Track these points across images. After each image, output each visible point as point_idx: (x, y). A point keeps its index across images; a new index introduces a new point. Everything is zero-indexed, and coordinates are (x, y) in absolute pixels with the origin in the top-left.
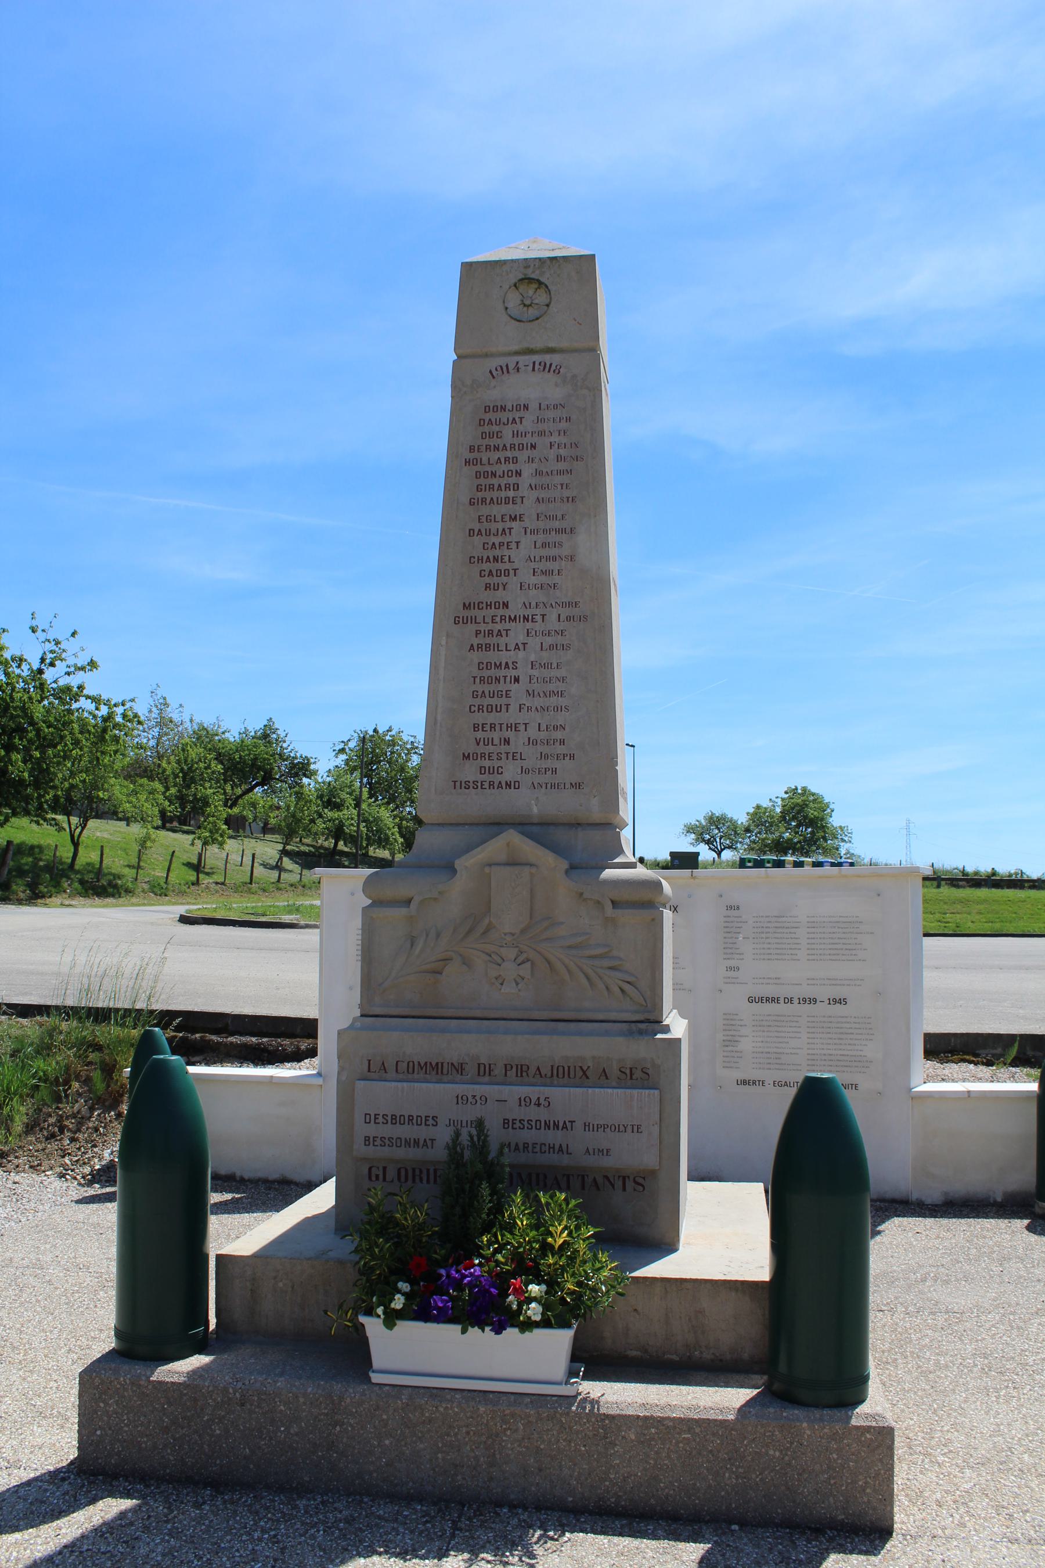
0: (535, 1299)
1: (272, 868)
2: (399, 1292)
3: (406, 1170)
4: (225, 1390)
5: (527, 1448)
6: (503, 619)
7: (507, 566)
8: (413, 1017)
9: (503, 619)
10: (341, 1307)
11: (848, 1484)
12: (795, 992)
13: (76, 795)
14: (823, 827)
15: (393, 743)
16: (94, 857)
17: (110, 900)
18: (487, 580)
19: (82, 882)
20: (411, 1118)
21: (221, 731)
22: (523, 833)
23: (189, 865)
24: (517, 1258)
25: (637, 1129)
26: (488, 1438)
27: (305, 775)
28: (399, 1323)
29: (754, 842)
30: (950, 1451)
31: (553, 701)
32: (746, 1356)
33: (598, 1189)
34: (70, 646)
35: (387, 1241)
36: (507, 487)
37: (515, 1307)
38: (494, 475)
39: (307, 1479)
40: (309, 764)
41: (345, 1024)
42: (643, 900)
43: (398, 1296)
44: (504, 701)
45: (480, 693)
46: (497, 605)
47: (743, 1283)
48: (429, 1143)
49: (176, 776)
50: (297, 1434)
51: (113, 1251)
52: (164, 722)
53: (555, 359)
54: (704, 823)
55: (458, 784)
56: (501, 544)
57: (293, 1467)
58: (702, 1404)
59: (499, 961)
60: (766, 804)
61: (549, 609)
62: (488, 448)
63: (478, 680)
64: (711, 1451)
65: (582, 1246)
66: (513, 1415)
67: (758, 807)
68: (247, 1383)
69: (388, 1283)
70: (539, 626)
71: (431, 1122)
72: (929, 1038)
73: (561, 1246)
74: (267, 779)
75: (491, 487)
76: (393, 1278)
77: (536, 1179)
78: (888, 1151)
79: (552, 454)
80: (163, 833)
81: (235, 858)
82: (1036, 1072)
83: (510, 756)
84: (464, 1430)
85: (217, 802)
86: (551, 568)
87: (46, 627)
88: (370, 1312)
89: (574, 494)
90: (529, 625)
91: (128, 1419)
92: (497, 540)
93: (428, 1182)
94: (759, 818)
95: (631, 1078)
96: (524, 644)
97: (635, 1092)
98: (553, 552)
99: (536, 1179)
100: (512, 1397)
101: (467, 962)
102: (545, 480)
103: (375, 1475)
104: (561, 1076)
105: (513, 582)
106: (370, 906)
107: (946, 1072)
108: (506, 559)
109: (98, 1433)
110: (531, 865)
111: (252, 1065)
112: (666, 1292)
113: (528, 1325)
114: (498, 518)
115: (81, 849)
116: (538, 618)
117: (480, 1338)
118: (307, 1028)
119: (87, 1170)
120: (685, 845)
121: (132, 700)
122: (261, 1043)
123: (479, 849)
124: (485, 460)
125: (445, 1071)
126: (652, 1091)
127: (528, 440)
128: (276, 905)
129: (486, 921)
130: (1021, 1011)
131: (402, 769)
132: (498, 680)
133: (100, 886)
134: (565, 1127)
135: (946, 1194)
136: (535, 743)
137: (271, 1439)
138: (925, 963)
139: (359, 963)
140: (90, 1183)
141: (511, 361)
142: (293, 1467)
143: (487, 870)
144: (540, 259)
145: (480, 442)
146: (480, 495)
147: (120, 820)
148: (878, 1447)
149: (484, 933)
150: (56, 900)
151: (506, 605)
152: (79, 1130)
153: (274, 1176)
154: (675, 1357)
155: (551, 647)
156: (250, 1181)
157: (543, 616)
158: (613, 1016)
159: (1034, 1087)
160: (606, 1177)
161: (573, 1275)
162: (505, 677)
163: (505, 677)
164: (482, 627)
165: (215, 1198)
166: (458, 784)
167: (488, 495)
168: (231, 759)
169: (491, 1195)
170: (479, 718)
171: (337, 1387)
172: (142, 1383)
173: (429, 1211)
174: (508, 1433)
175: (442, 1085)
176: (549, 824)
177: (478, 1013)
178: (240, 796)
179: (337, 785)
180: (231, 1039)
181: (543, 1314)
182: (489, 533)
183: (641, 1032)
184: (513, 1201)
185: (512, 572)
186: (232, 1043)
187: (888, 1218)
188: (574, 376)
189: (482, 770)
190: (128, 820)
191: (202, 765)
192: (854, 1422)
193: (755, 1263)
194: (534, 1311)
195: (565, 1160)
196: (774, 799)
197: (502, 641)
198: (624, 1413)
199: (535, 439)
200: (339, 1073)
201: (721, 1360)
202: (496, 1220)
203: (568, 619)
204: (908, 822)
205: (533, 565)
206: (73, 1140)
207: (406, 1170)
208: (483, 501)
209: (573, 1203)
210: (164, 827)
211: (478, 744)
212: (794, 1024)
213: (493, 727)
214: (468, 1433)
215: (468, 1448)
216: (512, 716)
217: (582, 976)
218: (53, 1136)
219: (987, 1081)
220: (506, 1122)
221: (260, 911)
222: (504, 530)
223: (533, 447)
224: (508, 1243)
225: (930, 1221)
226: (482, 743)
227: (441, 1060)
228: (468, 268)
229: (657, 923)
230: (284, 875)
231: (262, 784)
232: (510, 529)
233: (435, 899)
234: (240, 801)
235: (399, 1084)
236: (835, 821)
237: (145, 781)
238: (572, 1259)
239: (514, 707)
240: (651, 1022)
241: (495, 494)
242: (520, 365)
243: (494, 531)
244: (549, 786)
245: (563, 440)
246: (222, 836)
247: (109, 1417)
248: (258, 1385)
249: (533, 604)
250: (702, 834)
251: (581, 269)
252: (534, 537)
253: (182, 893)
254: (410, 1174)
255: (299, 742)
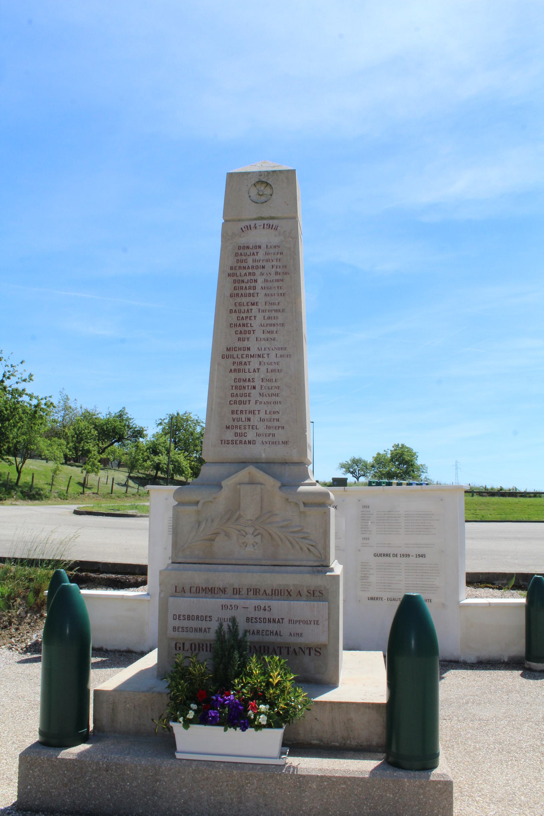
0: (263, 713)
1: (123, 485)
2: (191, 709)
3: (195, 645)
4: (98, 763)
5: (259, 793)
6: (247, 356)
7: (250, 328)
8: (199, 564)
9: (247, 356)
10: (160, 717)
11: (429, 812)
12: (399, 551)
13: (19, 447)
14: (412, 465)
15: (187, 420)
16: (29, 479)
17: (36, 502)
18: (239, 336)
19: (22, 492)
20: (198, 617)
21: (96, 413)
22: (257, 467)
23: (79, 483)
24: (254, 691)
25: (317, 623)
26: (238, 788)
27: (141, 437)
28: (191, 726)
29: (376, 472)
30: (483, 795)
31: (273, 399)
32: (374, 743)
33: (296, 654)
34: (20, 368)
35: (185, 682)
36: (250, 288)
37: (252, 717)
38: (243, 281)
39: (141, 811)
40: (143, 431)
41: (163, 568)
42: (319, 503)
43: (190, 712)
44: (247, 398)
45: (235, 394)
46: (244, 349)
47: (373, 704)
48: (207, 630)
49: (73, 437)
50: (136, 787)
51: (39, 689)
52: (67, 408)
53: (275, 222)
54: (350, 463)
55: (223, 442)
56: (246, 317)
57: (133, 805)
58: (351, 769)
59: (244, 534)
60: (382, 452)
61: (271, 351)
62: (240, 268)
63: (234, 388)
64: (356, 795)
65: (288, 684)
66: (251, 775)
67: (379, 454)
68: (110, 759)
69: (185, 704)
70: (266, 360)
71: (208, 619)
72: (468, 575)
73: (277, 684)
74: (121, 439)
75: (242, 288)
76: (188, 702)
77: (263, 649)
78: (449, 636)
79: (273, 271)
80: (65, 467)
81: (103, 480)
82: (525, 593)
83: (251, 427)
84: (225, 784)
85: (94, 450)
86: (272, 330)
87: (6, 359)
88: (176, 720)
89: (284, 292)
90: (261, 359)
91: (45, 779)
92: (244, 315)
93: (207, 651)
94: (379, 460)
95: (314, 596)
96: (258, 369)
97: (315, 603)
98: (274, 321)
99: (263, 649)
100: (251, 766)
101: (227, 535)
102: (269, 284)
103: (177, 809)
104: (277, 594)
105: (252, 337)
106: (177, 505)
107: (478, 593)
108: (249, 325)
109: (29, 787)
110: (261, 484)
111: (112, 589)
112: (332, 709)
113: (259, 727)
114: (245, 304)
115: (22, 475)
116: (266, 356)
117: (234, 733)
118: (142, 570)
119: (24, 645)
120: (340, 474)
121: (50, 397)
122: (118, 578)
123: (234, 476)
124: (238, 274)
125: (216, 592)
126: (324, 603)
127: (261, 264)
128: (125, 505)
129: (238, 513)
130: (517, 561)
131: (192, 434)
132: (244, 388)
133: (32, 494)
134: (279, 622)
135: (478, 657)
136: (263, 420)
137: (122, 789)
138: (466, 536)
139: (171, 536)
140: (25, 652)
141: (252, 223)
142: (133, 805)
143: (238, 486)
144: (267, 172)
145: (236, 264)
146: (236, 292)
147: (43, 459)
148: (445, 792)
149: (237, 519)
150: (8, 502)
151: (249, 349)
152: (20, 624)
153: (124, 648)
154: (337, 744)
155: (272, 371)
156: (111, 651)
157: (268, 354)
158: (304, 563)
159: (524, 600)
160: (301, 648)
161: (284, 699)
162: (248, 386)
163: (248, 386)
164: (236, 360)
165: (93, 660)
166: (223, 442)
167: (240, 292)
168: (102, 429)
169: (240, 657)
170: (235, 407)
171: (158, 761)
172: (53, 759)
173: (207, 666)
174: (249, 785)
175: (214, 599)
176: (270, 463)
177: (233, 562)
178: (107, 447)
179: (157, 442)
180: (102, 576)
181: (267, 721)
182: (240, 311)
183: (318, 572)
184: (251, 661)
185: (252, 332)
186: (102, 578)
187: (448, 670)
188: (285, 231)
189: (236, 434)
190: (47, 460)
191: (86, 431)
192: (432, 778)
193: (379, 693)
194: (263, 719)
195: (279, 639)
196: (386, 450)
197: (247, 367)
198: (310, 774)
199: (264, 264)
200: (160, 593)
201: (361, 746)
202: (242, 671)
203: (281, 356)
204: (457, 462)
205: (263, 328)
206: (17, 629)
207: (195, 645)
208: (237, 295)
209: (283, 661)
210: (66, 463)
211: (234, 421)
212: (398, 568)
213: (242, 412)
214: (227, 785)
215: (227, 793)
216: (252, 406)
217: (288, 542)
218: (5, 627)
219: (499, 597)
220: (248, 619)
221: (116, 508)
222: (248, 310)
223: (263, 267)
224: (249, 683)
225: (470, 672)
226: (236, 420)
227: (214, 586)
228: (231, 177)
229: (327, 515)
230: (129, 489)
231: (118, 441)
232: (251, 310)
233: (211, 502)
234: (106, 450)
235: (192, 599)
236: (419, 462)
237: (56, 439)
238: (283, 691)
239: (253, 402)
240: (324, 566)
241: (243, 292)
242: (257, 225)
243: (242, 310)
244: (271, 443)
245: (279, 264)
246: (97, 468)
247: (35, 779)
248: (116, 760)
249: (263, 349)
250: (349, 468)
251: (288, 177)
252: (263, 314)
253: (75, 498)
254: (197, 647)
255: (138, 422)
